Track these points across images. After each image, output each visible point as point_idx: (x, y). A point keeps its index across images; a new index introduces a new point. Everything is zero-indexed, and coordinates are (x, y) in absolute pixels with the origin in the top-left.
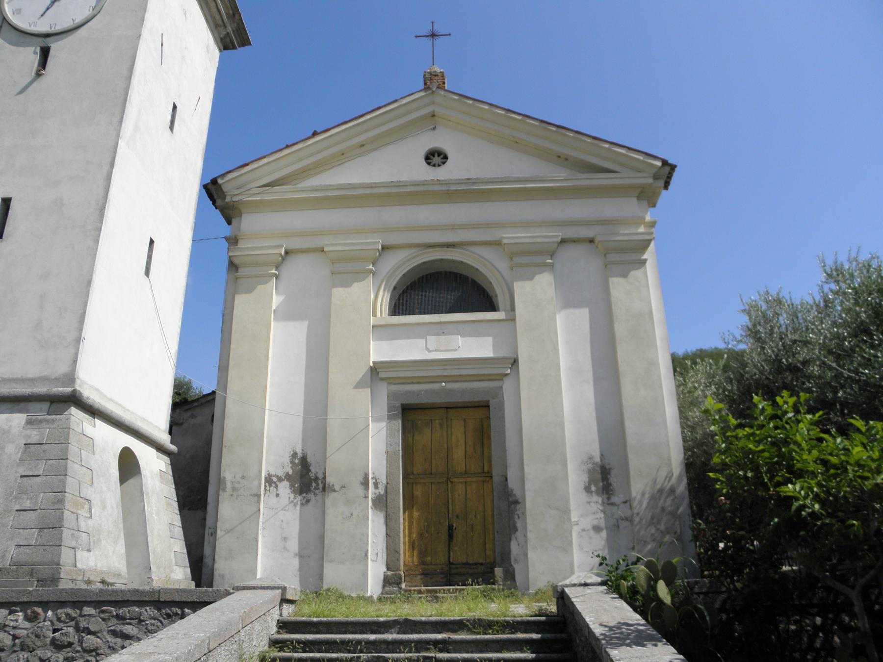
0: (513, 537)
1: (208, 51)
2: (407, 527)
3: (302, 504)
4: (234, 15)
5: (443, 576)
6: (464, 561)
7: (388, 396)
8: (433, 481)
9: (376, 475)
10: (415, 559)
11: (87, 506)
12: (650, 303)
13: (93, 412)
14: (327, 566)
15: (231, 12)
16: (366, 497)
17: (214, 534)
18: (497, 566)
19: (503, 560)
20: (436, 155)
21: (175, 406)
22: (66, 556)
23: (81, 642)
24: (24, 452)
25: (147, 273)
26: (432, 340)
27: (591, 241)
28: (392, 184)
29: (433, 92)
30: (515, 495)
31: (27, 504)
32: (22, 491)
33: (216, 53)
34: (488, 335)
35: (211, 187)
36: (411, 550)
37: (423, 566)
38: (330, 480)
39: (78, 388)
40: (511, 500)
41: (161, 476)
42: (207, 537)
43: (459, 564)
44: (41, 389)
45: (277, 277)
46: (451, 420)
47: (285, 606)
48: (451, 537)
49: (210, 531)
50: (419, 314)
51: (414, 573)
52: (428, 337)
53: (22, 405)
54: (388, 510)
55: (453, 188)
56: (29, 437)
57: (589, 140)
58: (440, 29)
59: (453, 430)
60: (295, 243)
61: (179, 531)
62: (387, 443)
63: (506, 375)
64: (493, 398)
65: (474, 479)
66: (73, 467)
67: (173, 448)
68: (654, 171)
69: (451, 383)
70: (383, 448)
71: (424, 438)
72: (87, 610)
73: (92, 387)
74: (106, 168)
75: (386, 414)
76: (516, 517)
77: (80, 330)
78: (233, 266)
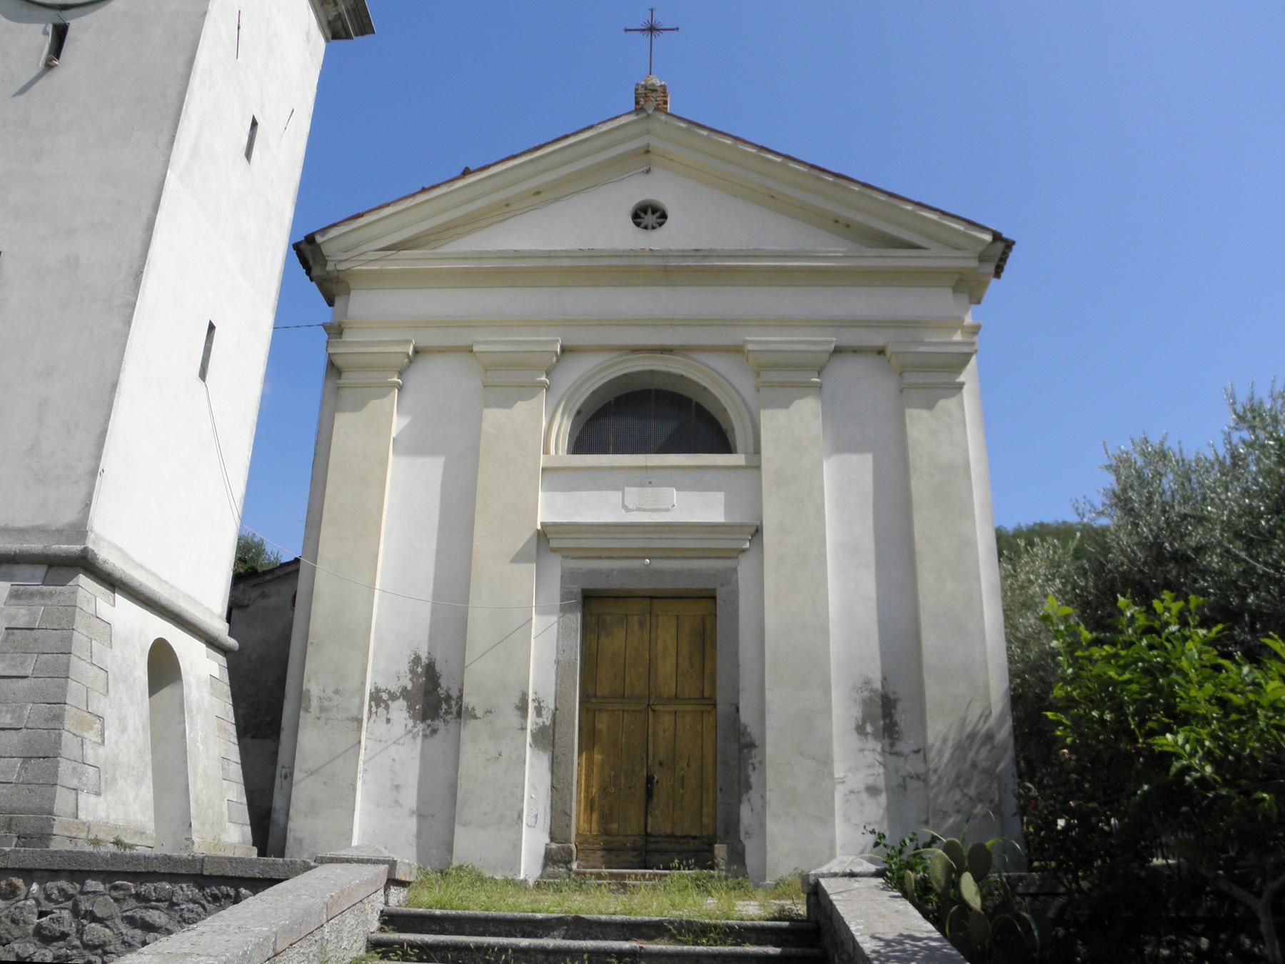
0: (745, 799)
1: (308, 40)
2: (583, 777)
3: (425, 736)
5: (635, 853)
6: (669, 832)
7: (562, 577)
8: (625, 708)
9: (540, 696)
10: (595, 826)
11: (97, 726)
12: (966, 450)
13: (113, 583)
14: (459, 831)
16: (523, 729)
17: (289, 776)
18: (718, 841)
19: (727, 832)
20: (650, 212)
21: (238, 579)
22: (62, 801)
23: (80, 932)
25: (203, 374)
26: (633, 494)
27: (881, 352)
29: (649, 115)
30: (749, 735)
33: (319, 43)
34: (718, 489)
36: (589, 812)
37: (606, 838)
38: (468, 700)
39: (90, 546)
40: (743, 741)
41: (212, 685)
42: (278, 781)
43: (660, 836)
44: (35, 546)
45: (400, 388)
46: (657, 616)
47: (393, 890)
48: (649, 794)
51: (592, 848)
52: (627, 489)
54: (556, 749)
55: (673, 263)
56: (14, 617)
57: (883, 198)
58: (662, 20)
59: (659, 631)
60: (429, 338)
61: (236, 770)
62: (557, 647)
63: (744, 551)
64: (722, 585)
65: (689, 708)
66: (79, 666)
67: (232, 643)
68: (981, 248)
70: (551, 655)
71: (615, 642)
72: (92, 885)
74: (146, 212)
75: (558, 603)
76: (751, 767)
77: (98, 457)
78: (334, 369)
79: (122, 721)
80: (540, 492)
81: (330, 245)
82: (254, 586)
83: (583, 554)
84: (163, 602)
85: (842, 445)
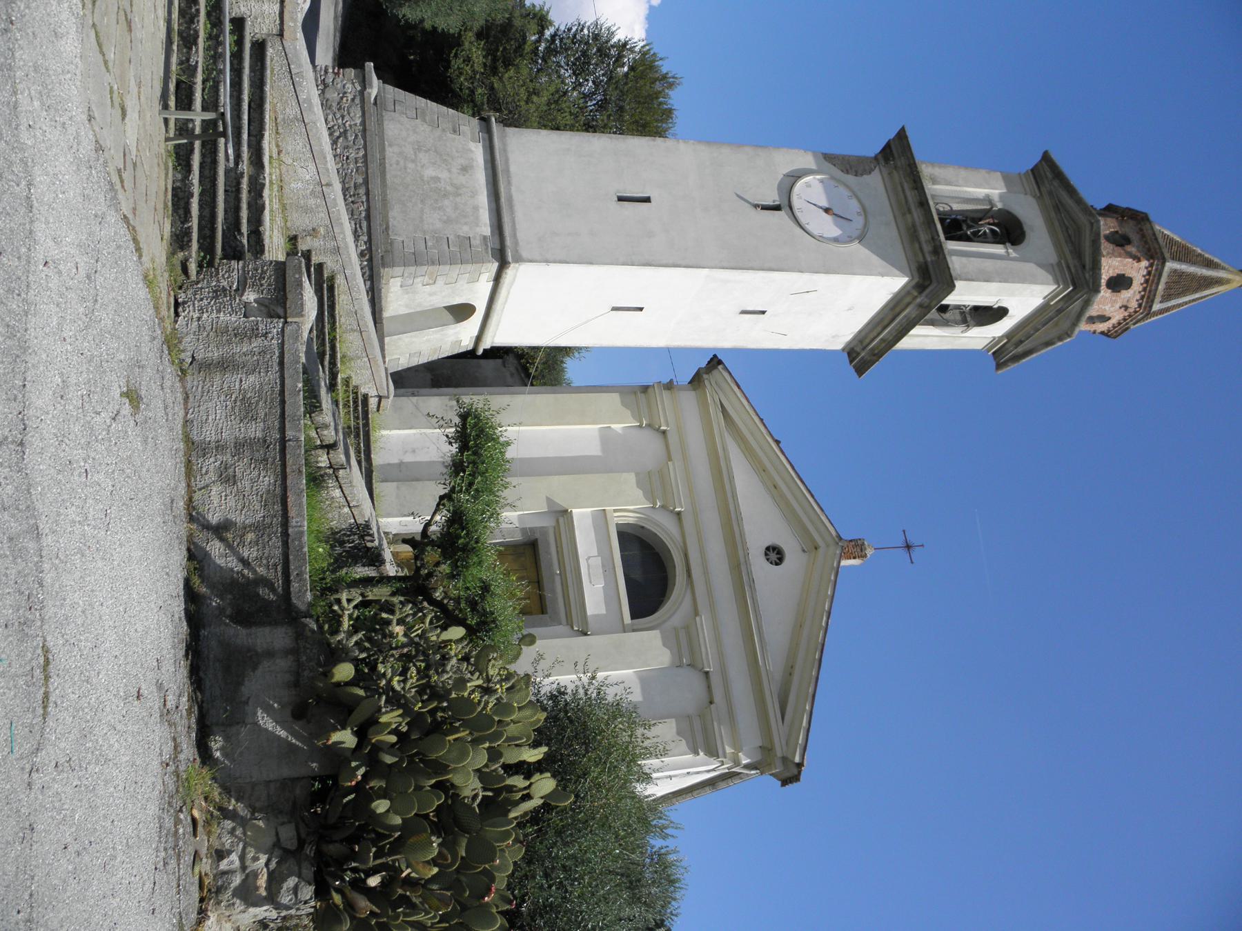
1: (833, 337)
3: (444, 462)
4: (874, 355)
11: (431, 282)
13: (497, 279)
14: (395, 484)
15: (876, 352)
17: (413, 395)
20: (778, 556)
21: (625, 632)
22: (398, 270)
24: (464, 237)
25: (615, 309)
26: (597, 561)
27: (711, 703)
28: (738, 514)
29: (838, 544)
31: (429, 244)
32: (438, 240)
33: (839, 345)
34: (607, 610)
35: (716, 360)
39: (512, 265)
41: (457, 341)
42: (411, 390)
44: (508, 242)
45: (640, 426)
47: (377, 399)
49: (416, 393)
50: (622, 556)
53: (497, 232)
55: (743, 568)
56: (475, 238)
57: (811, 690)
58: (916, 553)
60: (673, 439)
61: (415, 362)
63: (572, 628)
66: (456, 270)
67: (480, 352)
68: (790, 757)
69: (560, 581)
73: (515, 276)
75: (528, 526)
77: (555, 262)
78: (645, 389)
79: (434, 294)
80: (590, 510)
81: (719, 372)
82: (517, 370)
83: (558, 538)
84: (493, 307)
85: (644, 680)
